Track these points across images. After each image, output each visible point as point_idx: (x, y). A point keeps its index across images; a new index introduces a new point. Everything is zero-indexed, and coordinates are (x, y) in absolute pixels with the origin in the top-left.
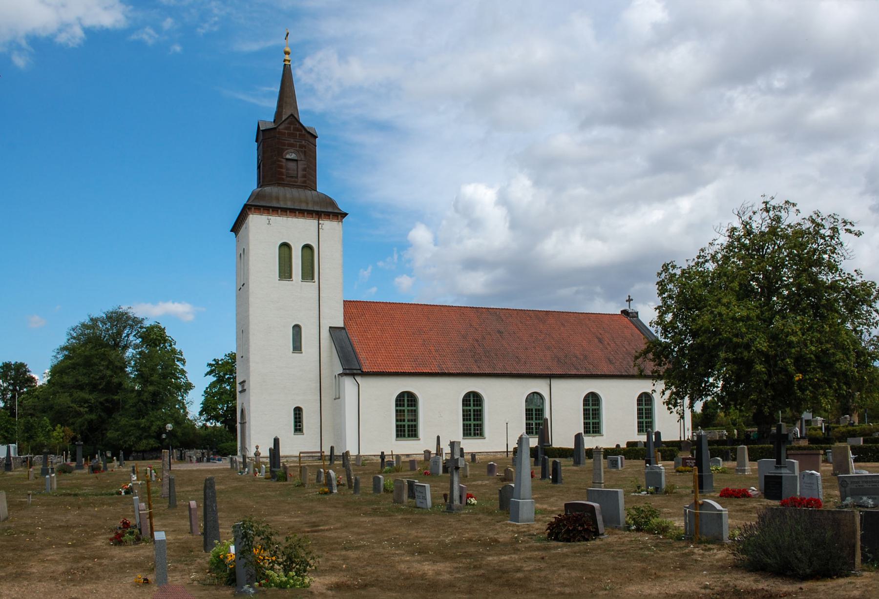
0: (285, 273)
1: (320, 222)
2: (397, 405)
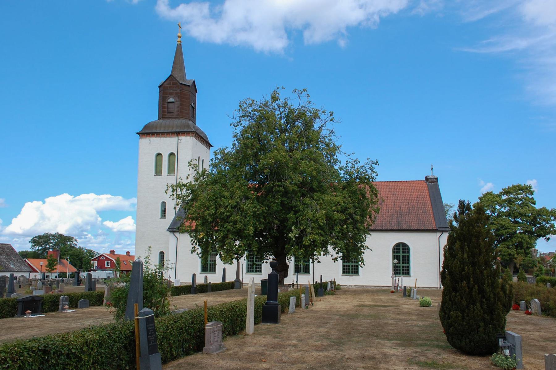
0: (158, 171)
1: (179, 138)
2: (394, 252)
